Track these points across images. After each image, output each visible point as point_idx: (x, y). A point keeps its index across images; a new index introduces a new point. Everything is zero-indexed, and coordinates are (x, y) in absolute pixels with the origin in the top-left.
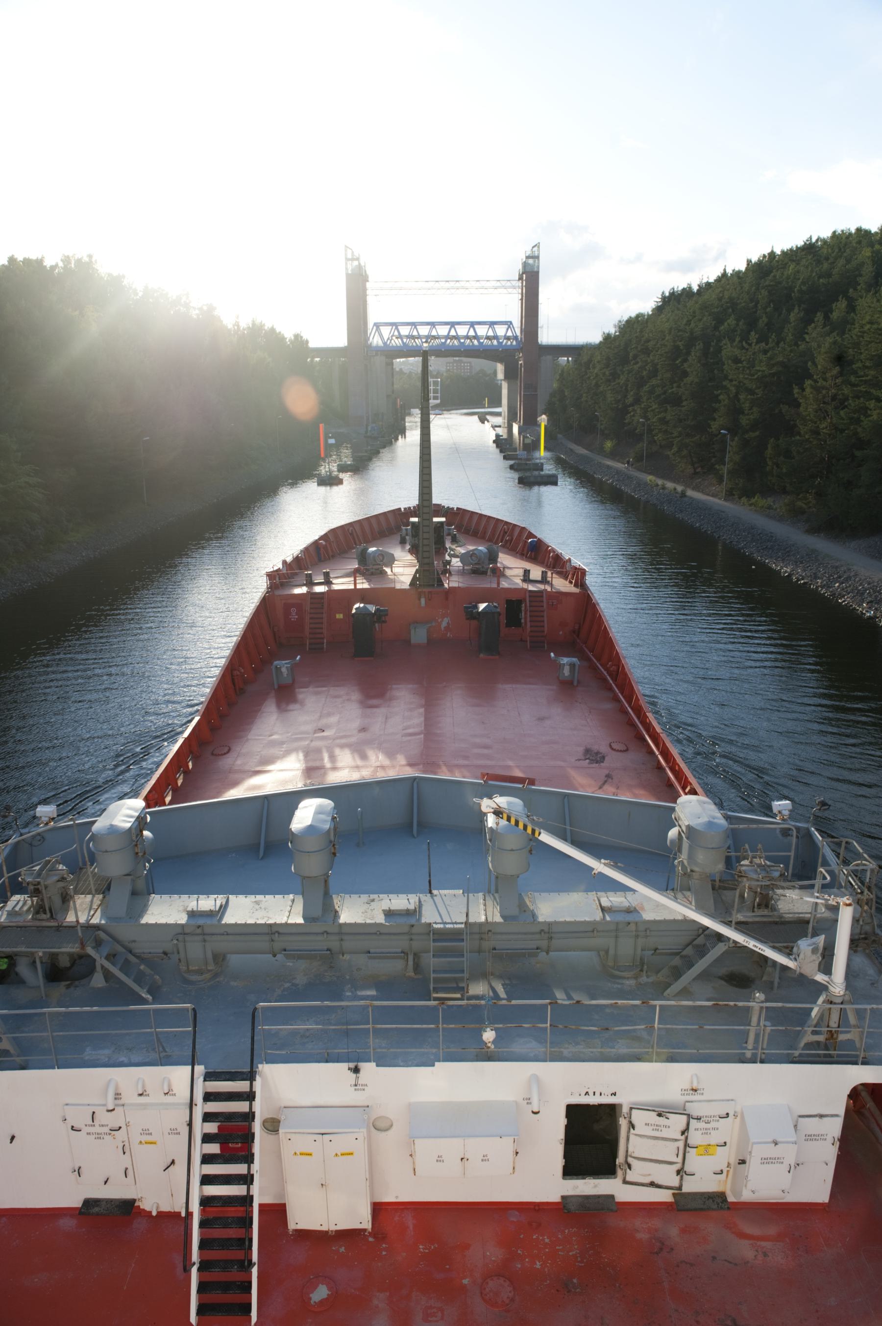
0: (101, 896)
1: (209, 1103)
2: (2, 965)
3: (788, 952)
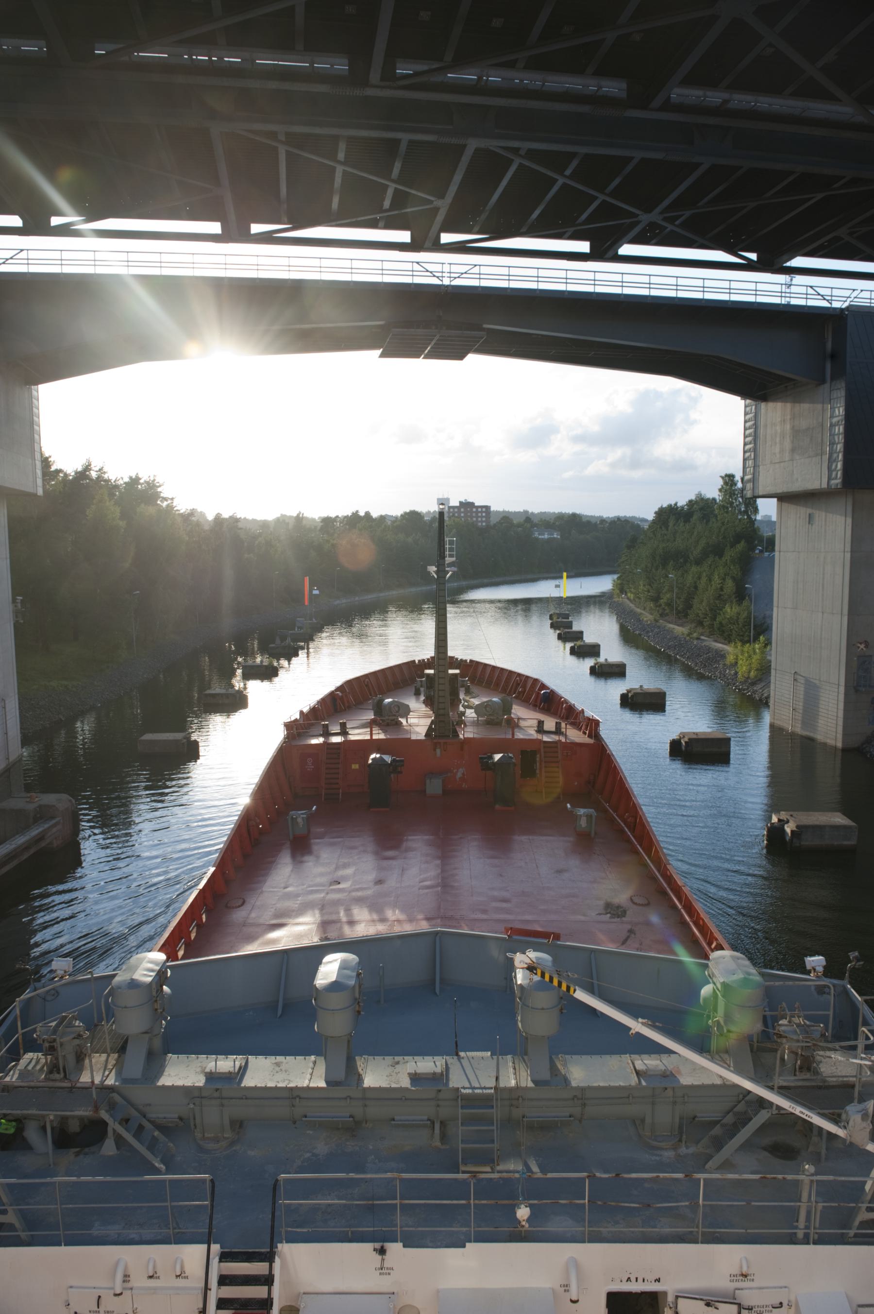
0: (116, 1055)
1: (223, 1288)
2: (7, 1128)
3: (836, 1119)
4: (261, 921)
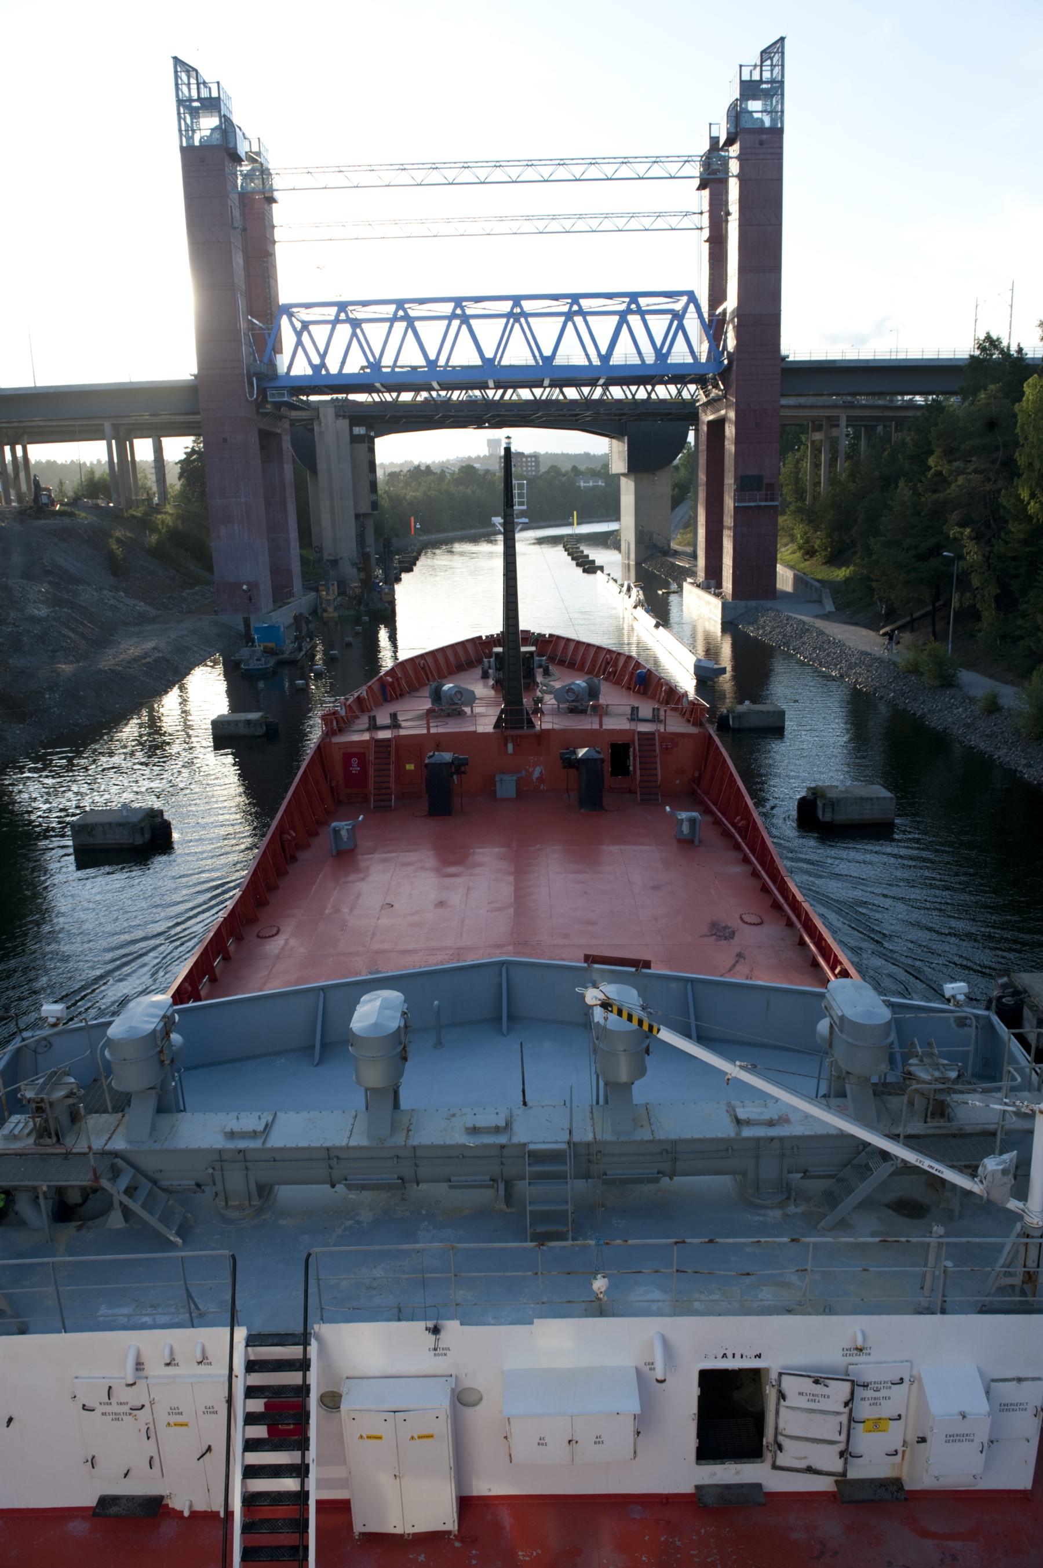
3: (972, 1171)
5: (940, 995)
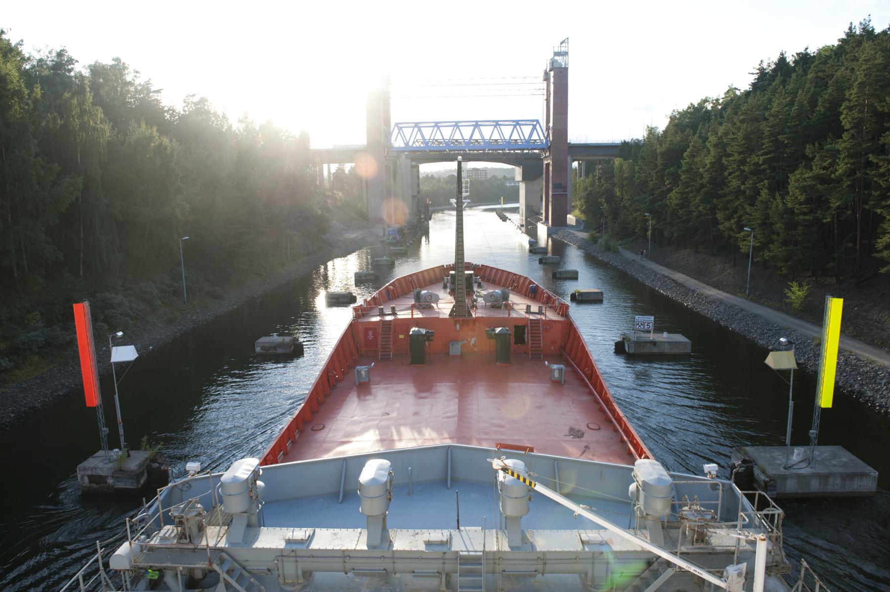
0: (226, 527)
3: (720, 575)
4: (335, 439)
5: (702, 472)
